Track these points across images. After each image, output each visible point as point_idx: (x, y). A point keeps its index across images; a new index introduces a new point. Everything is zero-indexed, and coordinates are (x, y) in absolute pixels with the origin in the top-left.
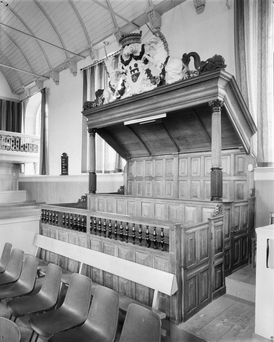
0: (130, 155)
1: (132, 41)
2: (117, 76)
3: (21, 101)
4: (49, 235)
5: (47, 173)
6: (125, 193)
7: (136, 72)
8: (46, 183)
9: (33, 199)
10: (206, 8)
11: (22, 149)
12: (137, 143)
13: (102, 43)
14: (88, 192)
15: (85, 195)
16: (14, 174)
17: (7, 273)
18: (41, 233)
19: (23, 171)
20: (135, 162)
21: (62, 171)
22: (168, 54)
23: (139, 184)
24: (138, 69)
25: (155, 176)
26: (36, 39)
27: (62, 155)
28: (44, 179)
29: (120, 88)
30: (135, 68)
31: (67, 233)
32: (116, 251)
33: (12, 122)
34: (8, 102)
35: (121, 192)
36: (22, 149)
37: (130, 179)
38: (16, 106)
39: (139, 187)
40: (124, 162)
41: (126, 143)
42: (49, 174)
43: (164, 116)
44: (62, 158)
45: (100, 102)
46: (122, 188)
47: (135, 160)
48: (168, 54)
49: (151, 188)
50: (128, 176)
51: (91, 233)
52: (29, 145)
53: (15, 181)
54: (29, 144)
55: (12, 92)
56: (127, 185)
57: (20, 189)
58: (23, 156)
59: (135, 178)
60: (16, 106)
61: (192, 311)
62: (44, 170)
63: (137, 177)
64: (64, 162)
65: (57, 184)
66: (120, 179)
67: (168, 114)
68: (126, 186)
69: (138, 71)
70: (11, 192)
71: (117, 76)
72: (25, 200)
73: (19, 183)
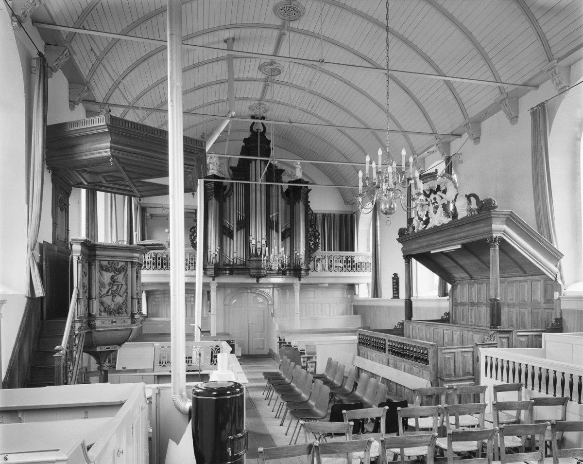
0: (454, 278)
1: (429, 179)
2: (422, 207)
3: (354, 213)
4: (363, 356)
5: (379, 295)
6: (451, 321)
7: (436, 204)
8: (379, 307)
9: (368, 325)
10: (519, 119)
11: (354, 269)
12: (455, 266)
13: (426, 152)
14: (404, 319)
15: (401, 322)
16: (349, 296)
17: (328, 377)
18: (359, 355)
19: (357, 293)
20: (459, 286)
21: (394, 294)
22: (457, 191)
23: (463, 310)
24: (437, 202)
25: (477, 302)
26: (371, 130)
27: (393, 276)
28: (376, 302)
29: (424, 218)
30: (434, 201)
31: (374, 354)
32: (403, 367)
33: (346, 237)
34: (341, 216)
35: (446, 319)
36: (354, 269)
37: (455, 304)
38: (349, 218)
39: (463, 314)
40: (449, 286)
41: (446, 266)
42: (381, 297)
43: (459, 247)
44: (393, 278)
45: (411, 230)
46: (448, 314)
47: (459, 284)
48: (457, 191)
49: (473, 316)
50: (453, 301)
51: (389, 354)
52: (361, 264)
53: (350, 304)
54: (361, 263)
55: (345, 203)
56: (453, 311)
57: (355, 313)
58: (353, 277)
59: (459, 304)
60: (349, 218)
61: (500, 442)
62: (376, 292)
63: (461, 302)
64: (395, 284)
65: (389, 308)
66: (445, 304)
67: (463, 245)
68: (451, 313)
69: (437, 203)
70: (345, 316)
71: (422, 207)
72: (360, 326)
73: (355, 306)
